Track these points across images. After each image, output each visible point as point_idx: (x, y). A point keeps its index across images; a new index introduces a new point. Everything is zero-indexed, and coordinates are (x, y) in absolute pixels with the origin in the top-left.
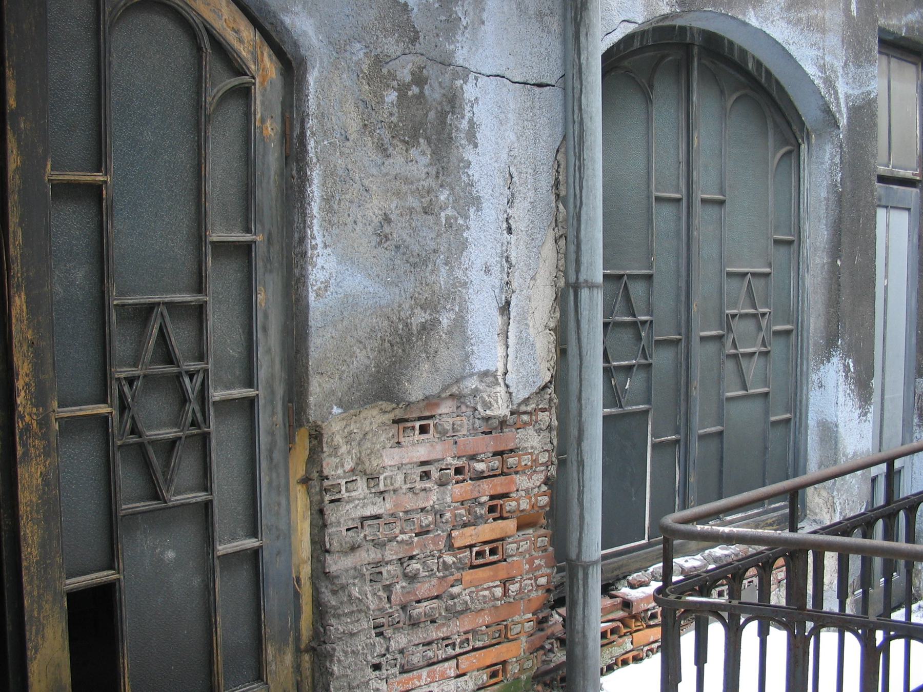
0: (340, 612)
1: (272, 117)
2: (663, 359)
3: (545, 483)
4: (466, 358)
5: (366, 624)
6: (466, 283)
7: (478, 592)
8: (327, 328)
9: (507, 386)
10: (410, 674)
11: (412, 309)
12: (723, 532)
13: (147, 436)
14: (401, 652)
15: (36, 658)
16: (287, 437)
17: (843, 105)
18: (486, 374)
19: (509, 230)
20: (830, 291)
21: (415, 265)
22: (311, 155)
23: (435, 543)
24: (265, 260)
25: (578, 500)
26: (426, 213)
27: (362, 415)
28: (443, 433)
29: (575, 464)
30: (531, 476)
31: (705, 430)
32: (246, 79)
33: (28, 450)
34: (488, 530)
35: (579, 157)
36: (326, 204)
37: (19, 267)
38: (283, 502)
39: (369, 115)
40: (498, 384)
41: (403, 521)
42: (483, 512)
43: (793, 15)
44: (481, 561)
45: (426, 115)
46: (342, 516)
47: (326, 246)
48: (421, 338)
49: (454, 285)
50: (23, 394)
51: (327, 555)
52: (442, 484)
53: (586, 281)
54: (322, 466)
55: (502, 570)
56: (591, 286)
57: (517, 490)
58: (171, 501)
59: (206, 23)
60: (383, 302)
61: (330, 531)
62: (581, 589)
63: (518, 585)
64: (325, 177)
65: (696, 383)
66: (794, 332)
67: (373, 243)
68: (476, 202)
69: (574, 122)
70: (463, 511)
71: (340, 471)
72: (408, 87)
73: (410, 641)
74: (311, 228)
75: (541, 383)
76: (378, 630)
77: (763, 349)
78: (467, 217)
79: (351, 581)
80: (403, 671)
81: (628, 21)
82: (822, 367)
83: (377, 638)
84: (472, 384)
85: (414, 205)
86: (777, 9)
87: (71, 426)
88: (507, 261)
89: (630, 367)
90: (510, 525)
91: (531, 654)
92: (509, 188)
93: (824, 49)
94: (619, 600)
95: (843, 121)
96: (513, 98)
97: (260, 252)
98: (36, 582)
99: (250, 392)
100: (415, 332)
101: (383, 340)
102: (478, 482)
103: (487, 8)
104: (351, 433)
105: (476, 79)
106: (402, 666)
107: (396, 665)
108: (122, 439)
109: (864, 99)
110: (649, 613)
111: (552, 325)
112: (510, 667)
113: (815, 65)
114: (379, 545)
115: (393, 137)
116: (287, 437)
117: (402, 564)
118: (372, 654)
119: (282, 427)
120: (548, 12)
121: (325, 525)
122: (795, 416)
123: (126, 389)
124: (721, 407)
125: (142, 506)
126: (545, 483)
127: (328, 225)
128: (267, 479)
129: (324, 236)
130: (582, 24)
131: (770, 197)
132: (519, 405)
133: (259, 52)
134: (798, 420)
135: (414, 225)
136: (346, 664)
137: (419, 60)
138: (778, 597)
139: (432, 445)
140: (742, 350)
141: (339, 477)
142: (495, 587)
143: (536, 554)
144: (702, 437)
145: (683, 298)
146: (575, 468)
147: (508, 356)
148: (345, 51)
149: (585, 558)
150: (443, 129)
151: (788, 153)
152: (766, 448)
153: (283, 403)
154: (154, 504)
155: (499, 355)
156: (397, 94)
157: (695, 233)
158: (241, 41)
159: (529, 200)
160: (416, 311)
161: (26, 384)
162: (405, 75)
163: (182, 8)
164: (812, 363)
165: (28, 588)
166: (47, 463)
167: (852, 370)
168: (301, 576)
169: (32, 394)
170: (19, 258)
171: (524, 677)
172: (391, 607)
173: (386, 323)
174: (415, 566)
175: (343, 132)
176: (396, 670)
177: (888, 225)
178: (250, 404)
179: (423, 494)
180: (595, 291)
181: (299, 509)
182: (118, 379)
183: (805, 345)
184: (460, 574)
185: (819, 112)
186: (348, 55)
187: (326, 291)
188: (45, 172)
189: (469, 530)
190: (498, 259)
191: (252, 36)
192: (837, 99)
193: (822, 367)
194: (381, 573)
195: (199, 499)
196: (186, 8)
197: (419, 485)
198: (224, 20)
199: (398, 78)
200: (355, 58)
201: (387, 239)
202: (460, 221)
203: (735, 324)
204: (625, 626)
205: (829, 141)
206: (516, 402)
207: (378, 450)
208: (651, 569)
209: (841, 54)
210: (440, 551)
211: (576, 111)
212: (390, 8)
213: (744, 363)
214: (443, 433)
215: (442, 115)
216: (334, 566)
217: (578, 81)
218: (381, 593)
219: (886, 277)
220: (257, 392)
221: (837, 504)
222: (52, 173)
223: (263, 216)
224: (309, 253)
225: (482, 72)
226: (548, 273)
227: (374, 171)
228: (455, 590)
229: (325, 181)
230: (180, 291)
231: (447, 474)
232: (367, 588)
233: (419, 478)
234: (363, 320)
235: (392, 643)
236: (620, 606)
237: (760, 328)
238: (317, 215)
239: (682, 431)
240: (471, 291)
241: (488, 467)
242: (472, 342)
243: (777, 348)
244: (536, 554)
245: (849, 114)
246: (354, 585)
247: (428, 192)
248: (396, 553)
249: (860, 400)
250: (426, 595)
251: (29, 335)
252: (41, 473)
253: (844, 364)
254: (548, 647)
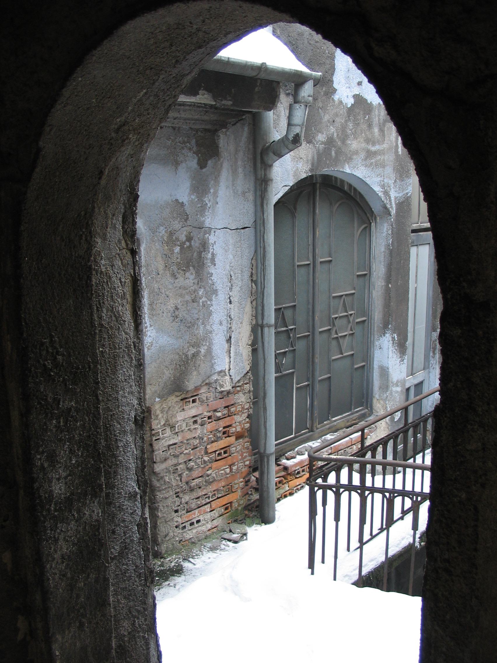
0: (161, 489)
2: (301, 346)
3: (247, 417)
4: (212, 366)
5: (171, 493)
6: (211, 331)
7: (219, 471)
9: (230, 376)
10: (191, 513)
11: (189, 348)
12: (334, 458)
14: (187, 503)
17: (393, 203)
18: (221, 372)
19: (230, 302)
20: (385, 300)
21: (189, 327)
22: (143, 285)
23: (200, 452)
25: (264, 425)
26: (193, 302)
27: (168, 399)
28: (202, 402)
29: (262, 409)
30: (241, 415)
31: (322, 377)
34: (222, 443)
35: (263, 264)
39: (168, 261)
40: (226, 375)
41: (186, 444)
42: (220, 435)
43: (368, 162)
44: (220, 457)
45: (193, 255)
46: (160, 445)
47: (151, 326)
48: (193, 361)
49: (206, 334)
51: (154, 464)
52: (202, 425)
53: (267, 324)
54: (151, 425)
55: (229, 460)
56: (269, 326)
57: (235, 423)
60: (176, 347)
62: (266, 466)
63: (236, 466)
64: (150, 294)
65: (317, 355)
66: (367, 321)
67: (171, 321)
68: (215, 292)
69: (261, 247)
70: (211, 436)
71: (159, 426)
72: (184, 243)
73: (190, 498)
74: (144, 319)
75: (245, 372)
76: (176, 495)
77: (351, 332)
78: (211, 300)
79: (165, 474)
80: (188, 512)
81: (286, 186)
82: (381, 338)
83: (177, 498)
84: (215, 377)
85: (188, 299)
86: (360, 161)
88: (230, 317)
89: (285, 353)
90: (233, 439)
91: (243, 497)
92: (230, 282)
93: (384, 176)
94: (282, 467)
95: (393, 212)
96: (231, 238)
100: (190, 358)
101: (176, 364)
102: (218, 422)
103: (219, 195)
104: (163, 408)
105: (215, 232)
106: (187, 509)
107: (184, 509)
109: (404, 197)
110: (296, 471)
111: (250, 343)
112: (233, 504)
113: (379, 185)
114: (176, 456)
115: (178, 269)
117: (186, 463)
118: (174, 505)
120: (248, 190)
121: (153, 451)
122: (367, 364)
124: (330, 365)
126: (247, 417)
127: (152, 316)
130: (265, 199)
131: (355, 254)
132: (236, 383)
134: (368, 365)
135: (188, 309)
136: (164, 512)
137: (188, 229)
138: (356, 481)
139: (198, 408)
140: (340, 335)
141: (159, 429)
142: (226, 468)
143: (244, 451)
144: (320, 381)
145: (311, 314)
146: (262, 411)
147: (230, 362)
148: (157, 232)
149: (268, 452)
150: (200, 260)
151: (365, 228)
152: (352, 382)
155: (227, 362)
156: (179, 248)
157: (317, 281)
159: (239, 286)
160: (190, 348)
162: (183, 238)
164: (376, 336)
167: (396, 339)
171: (240, 508)
172: (182, 484)
173: (177, 356)
174: (192, 464)
175: (157, 271)
176: (184, 512)
177: (417, 255)
179: (194, 431)
180: (271, 328)
183: (372, 327)
184: (210, 465)
185: (381, 208)
186: (157, 234)
189: (215, 444)
190: (226, 317)
192: (390, 201)
193: (381, 338)
194: (177, 469)
197: (193, 427)
199: (180, 240)
200: (161, 234)
201: (177, 317)
202: (209, 303)
203: (337, 322)
204: (285, 479)
205: (386, 222)
206: (234, 382)
207: (175, 414)
208: (296, 449)
209: (393, 176)
210: (202, 455)
211: (262, 242)
212: (175, 206)
213: (341, 340)
214: (202, 402)
215: (200, 253)
217: (263, 227)
218: (177, 478)
219: (416, 282)
221: (388, 407)
224: (144, 330)
225: (218, 228)
226: (248, 319)
227: (171, 287)
228: (209, 472)
231: (205, 420)
232: (172, 477)
233: (192, 424)
234: (167, 356)
235: (183, 499)
236: (282, 470)
237: (349, 322)
238: (147, 312)
239: (311, 380)
240: (214, 335)
241: (222, 414)
242: (215, 358)
243: (358, 330)
244: (244, 451)
245: (396, 207)
246: (166, 476)
247: (194, 292)
248: (183, 459)
249: (400, 354)
250: (197, 476)
253: (392, 337)
254: (250, 493)
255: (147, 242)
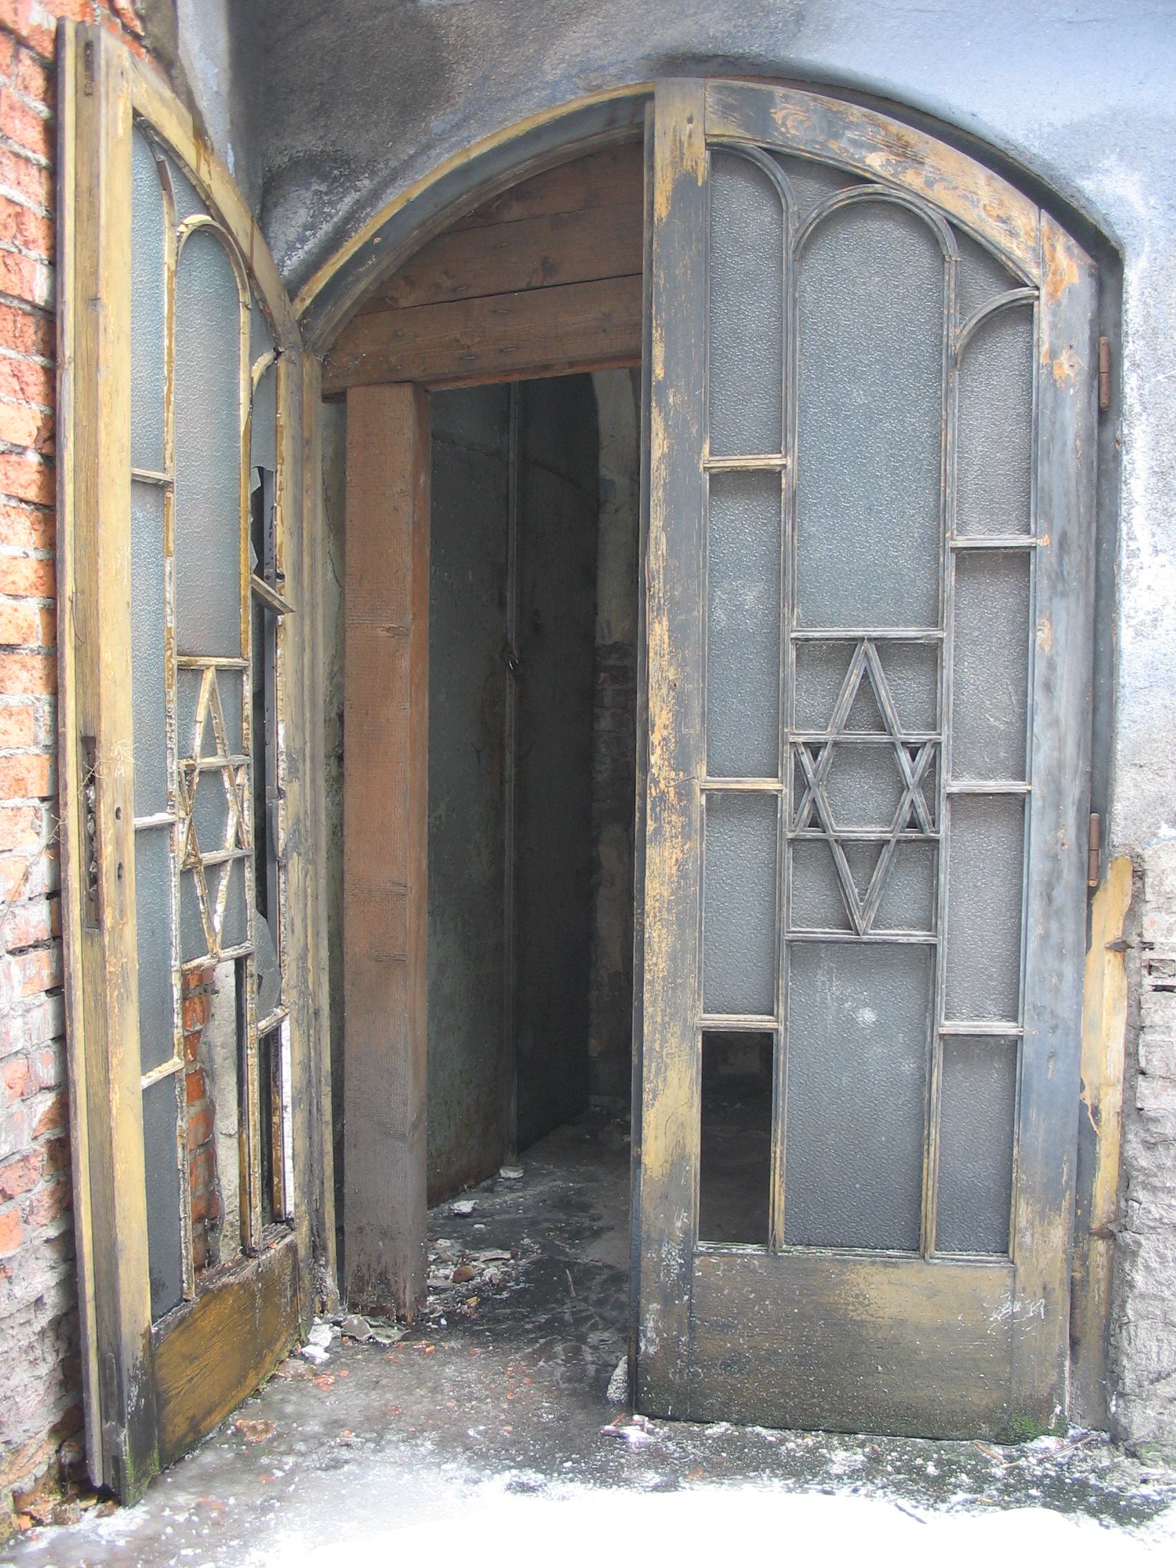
0: (1156, 1182)
1: (1071, 347)
8: (1156, 689)
13: (835, 831)
15: (653, 1105)
16: (1082, 868)
24: (1054, 577)
32: (1025, 291)
33: (661, 827)
36: (1158, 480)
37: (661, 584)
38: (1069, 971)
47: (1156, 552)
50: (658, 751)
51: (1141, 1077)
58: (865, 933)
59: (951, 218)
61: (1149, 1038)
87: (720, 804)
97: (1042, 565)
98: (660, 1004)
99: (1019, 787)
108: (794, 831)
116: (1082, 868)
119: (1074, 848)
123: (806, 759)
125: (820, 933)
128: (1039, 930)
129: (1153, 535)
133: (1047, 247)
153: (1079, 810)
154: (841, 934)
158: (1012, 234)
161: (664, 739)
163: (909, 202)
165: (650, 1010)
166: (686, 847)
168: (1101, 1106)
169: (671, 753)
170: (662, 572)
178: (1016, 805)
181: (1106, 993)
182: (794, 744)
187: (1155, 627)
188: (700, 458)
191: (1034, 223)
195: (913, 940)
196: (917, 201)
198: (981, 208)
216: (1152, 1100)
220: (1029, 788)
222: (711, 459)
223: (1051, 506)
229: (1157, 443)
230: (906, 623)
238: (1142, 501)
251: (671, 675)
252: (677, 860)
255: (1157, 251)
